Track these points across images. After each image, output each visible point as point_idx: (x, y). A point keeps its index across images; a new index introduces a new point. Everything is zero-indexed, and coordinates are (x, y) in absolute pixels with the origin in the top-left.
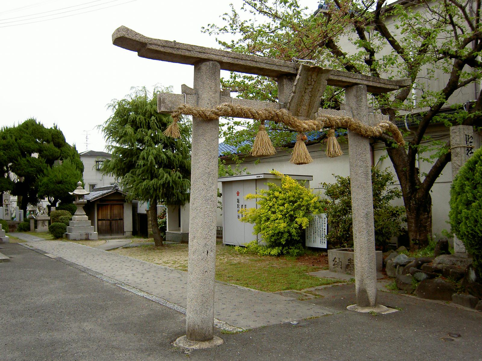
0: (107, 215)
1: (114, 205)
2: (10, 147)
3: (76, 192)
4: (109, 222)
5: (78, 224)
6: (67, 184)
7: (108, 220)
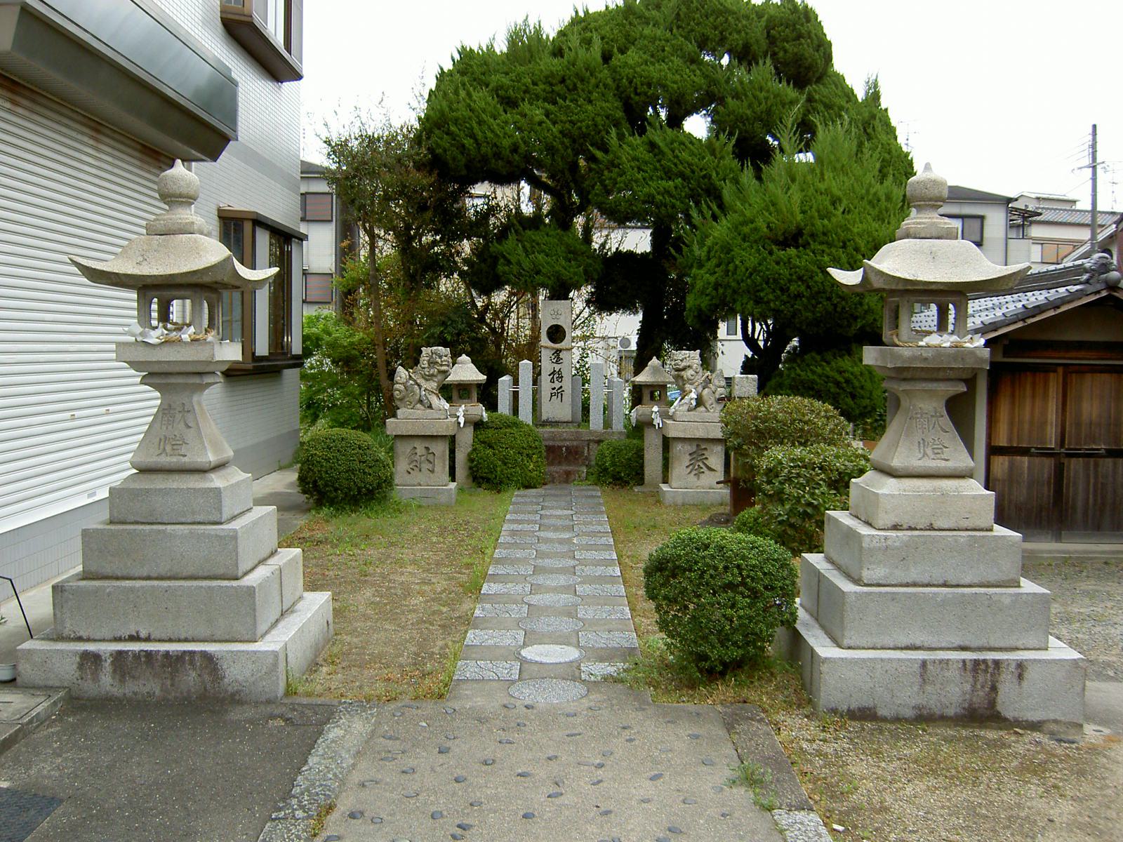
0: (1043, 424)
1: (1083, 370)
2: (575, 88)
3: (897, 261)
4: (1048, 463)
5: (903, 556)
6: (830, 245)
7: (1046, 453)
